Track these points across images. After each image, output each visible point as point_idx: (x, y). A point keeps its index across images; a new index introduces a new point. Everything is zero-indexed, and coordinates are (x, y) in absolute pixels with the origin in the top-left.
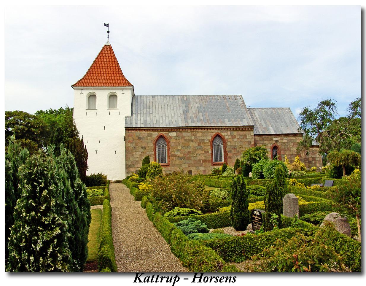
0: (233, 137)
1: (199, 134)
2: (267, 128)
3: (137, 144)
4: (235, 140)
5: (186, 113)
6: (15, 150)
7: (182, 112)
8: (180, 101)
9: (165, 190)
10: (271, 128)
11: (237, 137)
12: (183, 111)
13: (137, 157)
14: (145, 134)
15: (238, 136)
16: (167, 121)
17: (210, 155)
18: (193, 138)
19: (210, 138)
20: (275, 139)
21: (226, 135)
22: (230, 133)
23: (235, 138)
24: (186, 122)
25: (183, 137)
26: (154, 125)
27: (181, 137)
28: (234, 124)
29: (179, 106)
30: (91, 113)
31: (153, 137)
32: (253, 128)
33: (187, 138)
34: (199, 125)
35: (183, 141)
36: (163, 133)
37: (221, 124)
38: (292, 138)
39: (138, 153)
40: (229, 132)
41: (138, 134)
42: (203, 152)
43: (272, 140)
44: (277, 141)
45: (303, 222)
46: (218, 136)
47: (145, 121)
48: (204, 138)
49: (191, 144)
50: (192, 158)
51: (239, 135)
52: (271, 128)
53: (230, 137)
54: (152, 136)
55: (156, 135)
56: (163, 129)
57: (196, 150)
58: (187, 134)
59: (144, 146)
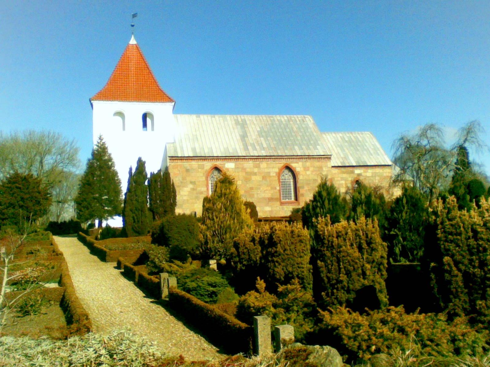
0: (306, 169)
1: (264, 165)
2: (346, 158)
3: (184, 179)
4: (308, 173)
5: (244, 137)
6: (226, 186)
7: (239, 138)
8: (234, 122)
9: (217, 239)
10: (351, 158)
11: (311, 169)
12: (240, 135)
13: (185, 195)
14: (194, 164)
15: (312, 168)
16: (222, 150)
17: (278, 191)
18: (256, 170)
19: (277, 170)
20: (357, 171)
21: (297, 166)
22: (302, 165)
23: (308, 170)
24: (246, 148)
25: (244, 169)
26: (207, 153)
27: (240, 170)
28: (288, 153)
29: (234, 129)
30: (101, 134)
31: (205, 169)
32: (330, 158)
33: (248, 170)
34: (264, 153)
35: (244, 174)
36: (218, 163)
37: (263, 152)
38: (378, 170)
39: (186, 189)
40: (300, 163)
41: (186, 164)
42: (270, 188)
43: (353, 172)
44: (359, 175)
45: (245, 301)
46: (288, 168)
47: (194, 149)
48: (270, 170)
49: (254, 178)
50: (255, 196)
51: (314, 167)
52: (351, 158)
53: (302, 169)
54: (204, 168)
55: (208, 165)
56: (218, 158)
57: (260, 185)
58: (249, 165)
59: (193, 180)
